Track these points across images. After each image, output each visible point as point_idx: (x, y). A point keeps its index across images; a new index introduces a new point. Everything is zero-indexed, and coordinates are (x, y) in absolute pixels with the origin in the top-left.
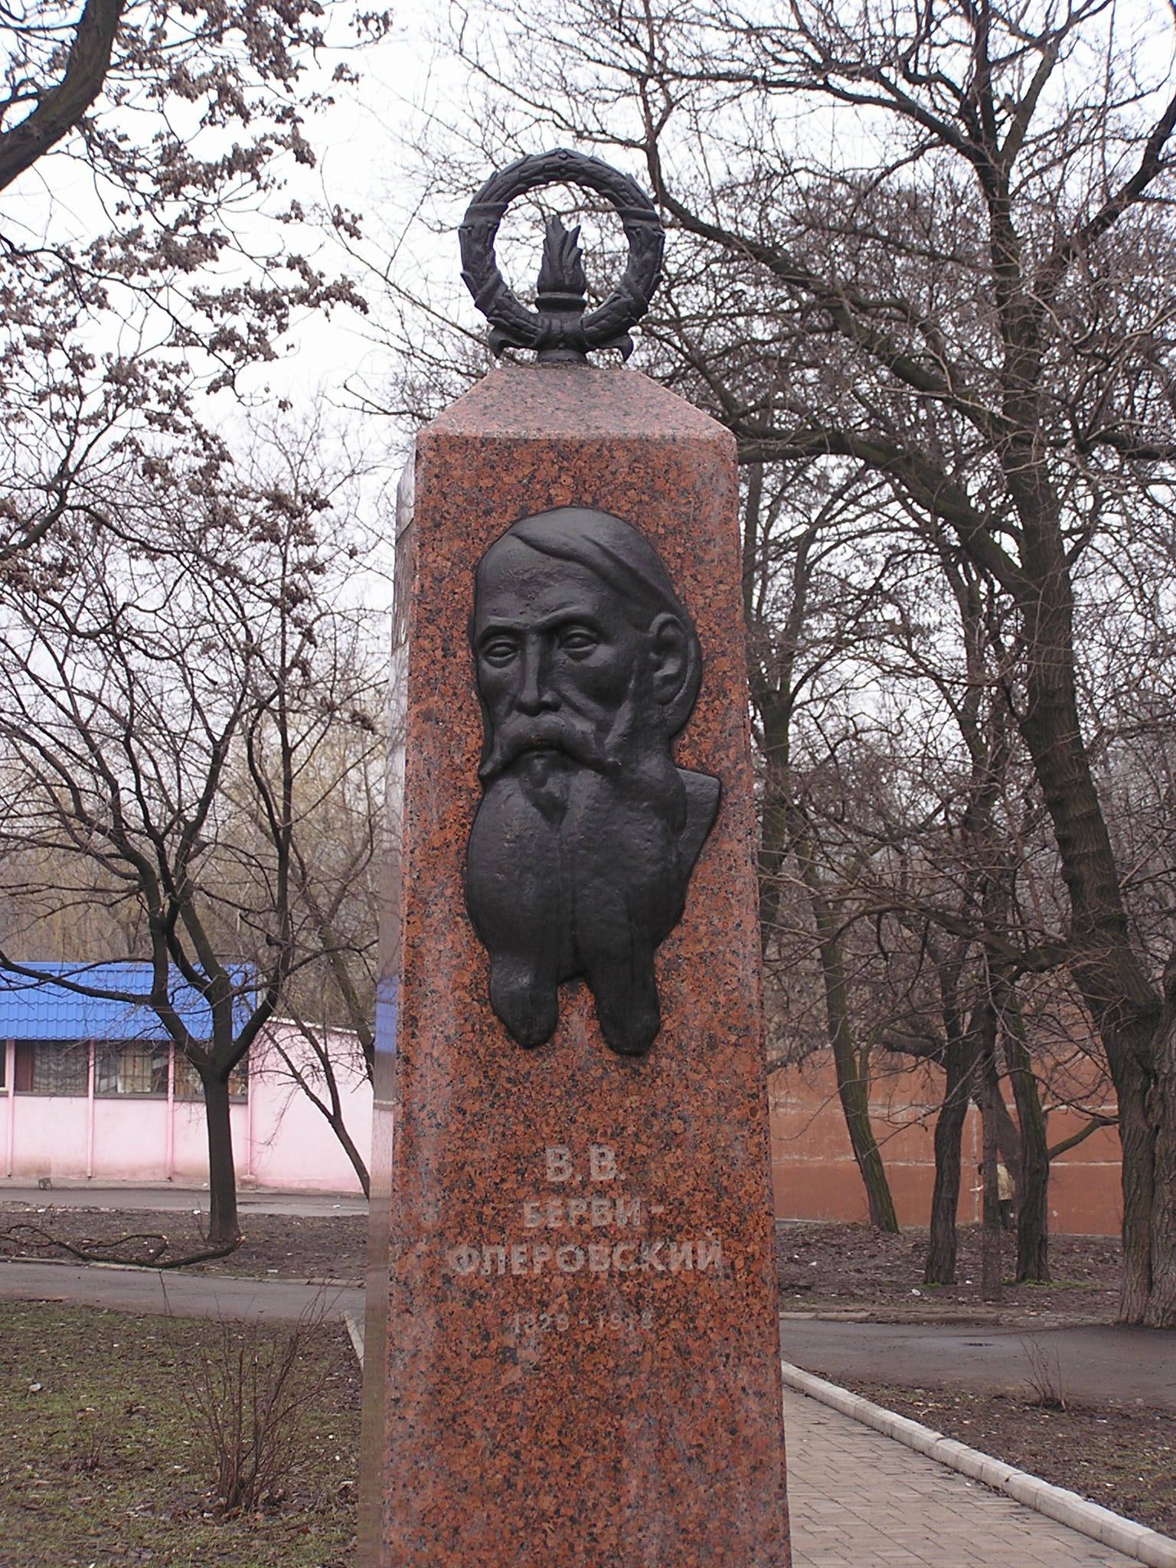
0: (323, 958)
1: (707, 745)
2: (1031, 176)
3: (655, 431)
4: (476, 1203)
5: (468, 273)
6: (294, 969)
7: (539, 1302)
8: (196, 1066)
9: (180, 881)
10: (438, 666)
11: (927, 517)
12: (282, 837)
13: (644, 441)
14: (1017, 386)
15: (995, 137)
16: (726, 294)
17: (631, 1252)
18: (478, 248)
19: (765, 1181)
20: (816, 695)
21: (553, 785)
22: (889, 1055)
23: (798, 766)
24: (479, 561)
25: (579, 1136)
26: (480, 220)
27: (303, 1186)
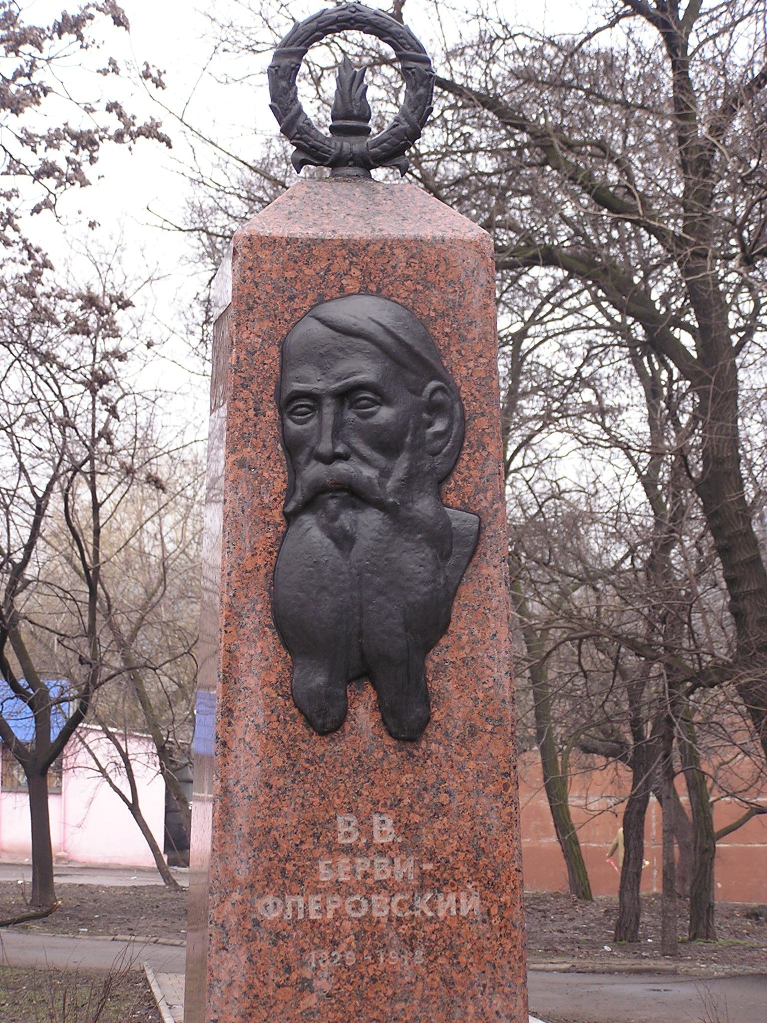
0: (125, 674)
1: (469, 489)
2: (706, 40)
3: (427, 232)
4: (280, 861)
5: (275, 105)
6: (101, 684)
7: (331, 942)
8: (21, 762)
9: (9, 611)
10: (251, 423)
11: (618, 319)
12: (92, 577)
13: (419, 241)
14: (696, 210)
15: (678, 9)
16: (457, 135)
17: (406, 901)
18: (284, 83)
19: (515, 844)
20: (527, 462)
21: (346, 519)
22: (584, 757)
23: (513, 520)
24: (285, 338)
25: (364, 807)
26: (285, 62)
27: (107, 861)
